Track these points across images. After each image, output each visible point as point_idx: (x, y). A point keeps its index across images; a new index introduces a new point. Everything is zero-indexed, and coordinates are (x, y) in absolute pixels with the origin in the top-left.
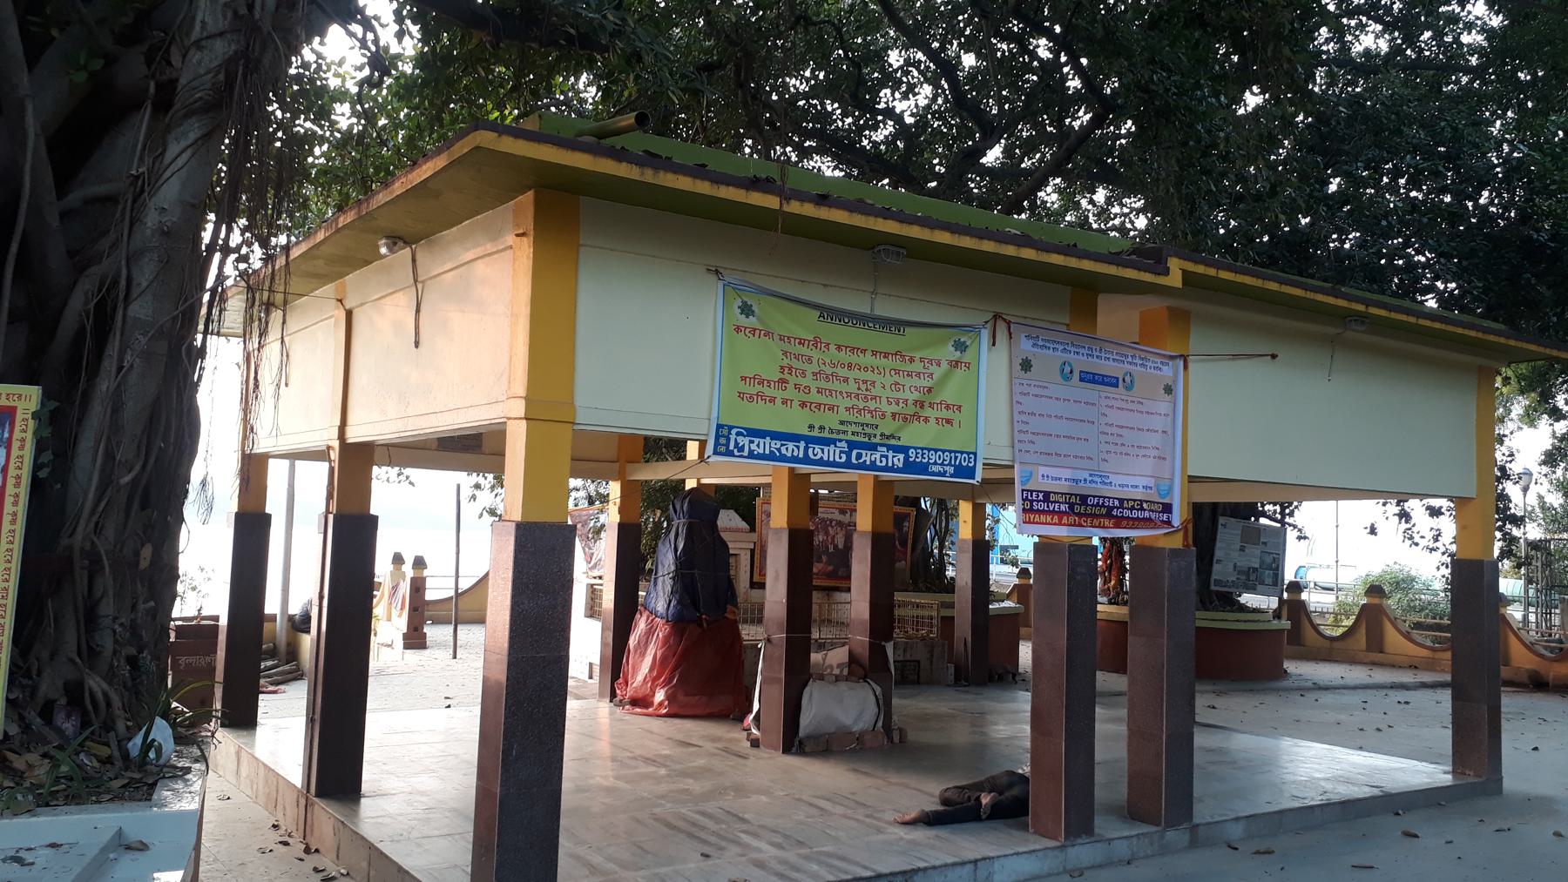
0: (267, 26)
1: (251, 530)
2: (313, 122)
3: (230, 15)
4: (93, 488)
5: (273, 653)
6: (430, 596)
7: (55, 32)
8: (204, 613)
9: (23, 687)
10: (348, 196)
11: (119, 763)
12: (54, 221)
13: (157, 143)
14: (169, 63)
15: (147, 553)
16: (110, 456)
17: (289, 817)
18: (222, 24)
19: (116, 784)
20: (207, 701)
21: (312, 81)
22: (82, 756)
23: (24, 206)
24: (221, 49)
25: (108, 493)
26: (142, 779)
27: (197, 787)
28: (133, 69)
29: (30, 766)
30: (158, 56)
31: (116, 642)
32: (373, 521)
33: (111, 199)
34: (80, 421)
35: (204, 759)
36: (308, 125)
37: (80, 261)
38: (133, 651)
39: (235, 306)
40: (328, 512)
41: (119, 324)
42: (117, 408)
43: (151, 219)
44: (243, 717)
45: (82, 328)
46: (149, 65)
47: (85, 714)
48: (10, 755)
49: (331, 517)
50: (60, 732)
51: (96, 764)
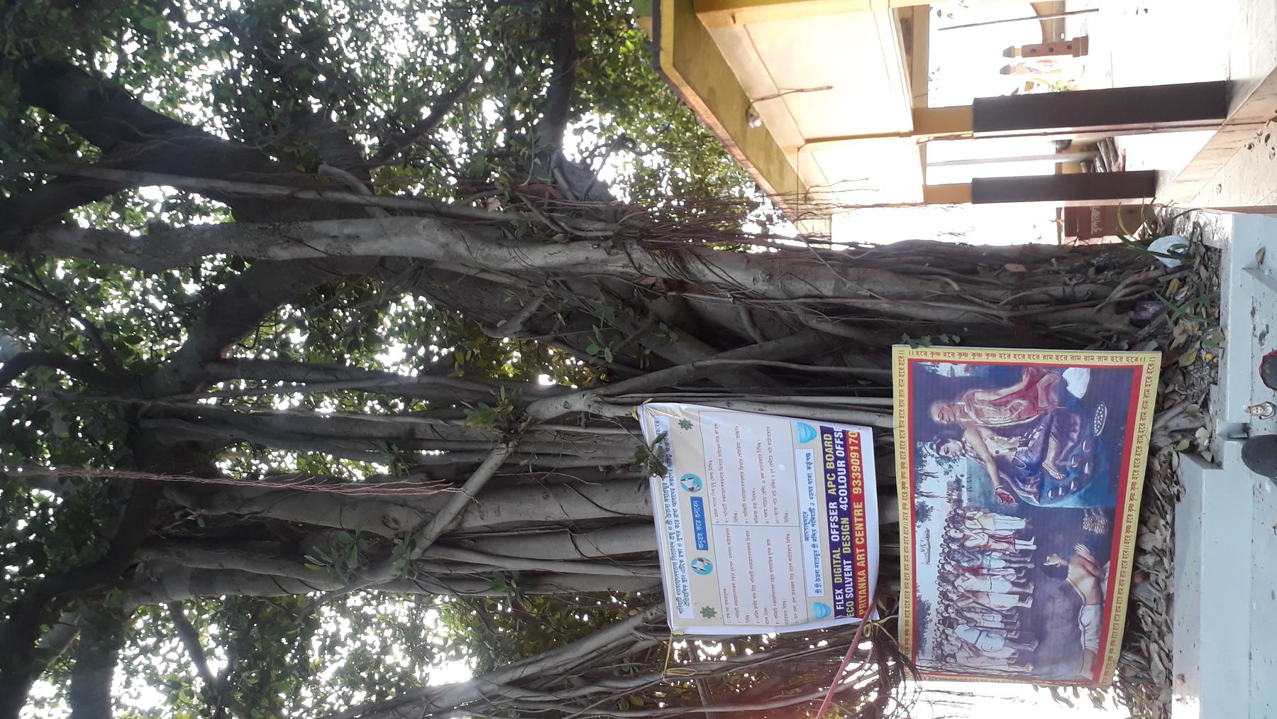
0: (616, 227)
1: (984, 192)
2: (661, 180)
3: (614, 251)
4: (963, 307)
5: (1089, 163)
6: (1037, 39)
7: (647, 352)
8: (1055, 217)
9: (1119, 339)
10: (711, 149)
11: (1186, 273)
12: (773, 344)
13: (706, 288)
14: (653, 285)
15: (1011, 267)
16: (938, 298)
17: (1241, 137)
18: (622, 255)
19: (1203, 273)
20: (1133, 210)
21: (632, 186)
22: (1178, 298)
23: (765, 363)
24: (638, 254)
25: (968, 297)
26: (1202, 258)
27: (1212, 217)
28: (660, 306)
29: (1184, 332)
30: (651, 292)
31: (1084, 282)
32: (978, 103)
33: (751, 313)
34: (912, 319)
35: (1186, 214)
36: (664, 184)
37: (796, 327)
38: (1091, 271)
39: (812, 226)
40: (972, 137)
41: (839, 301)
42: (900, 297)
43: (761, 287)
44: (1147, 182)
45: (845, 322)
46: (656, 297)
47: (1142, 299)
48: (1175, 344)
49: (976, 135)
50: (1155, 315)
51: (1186, 288)
